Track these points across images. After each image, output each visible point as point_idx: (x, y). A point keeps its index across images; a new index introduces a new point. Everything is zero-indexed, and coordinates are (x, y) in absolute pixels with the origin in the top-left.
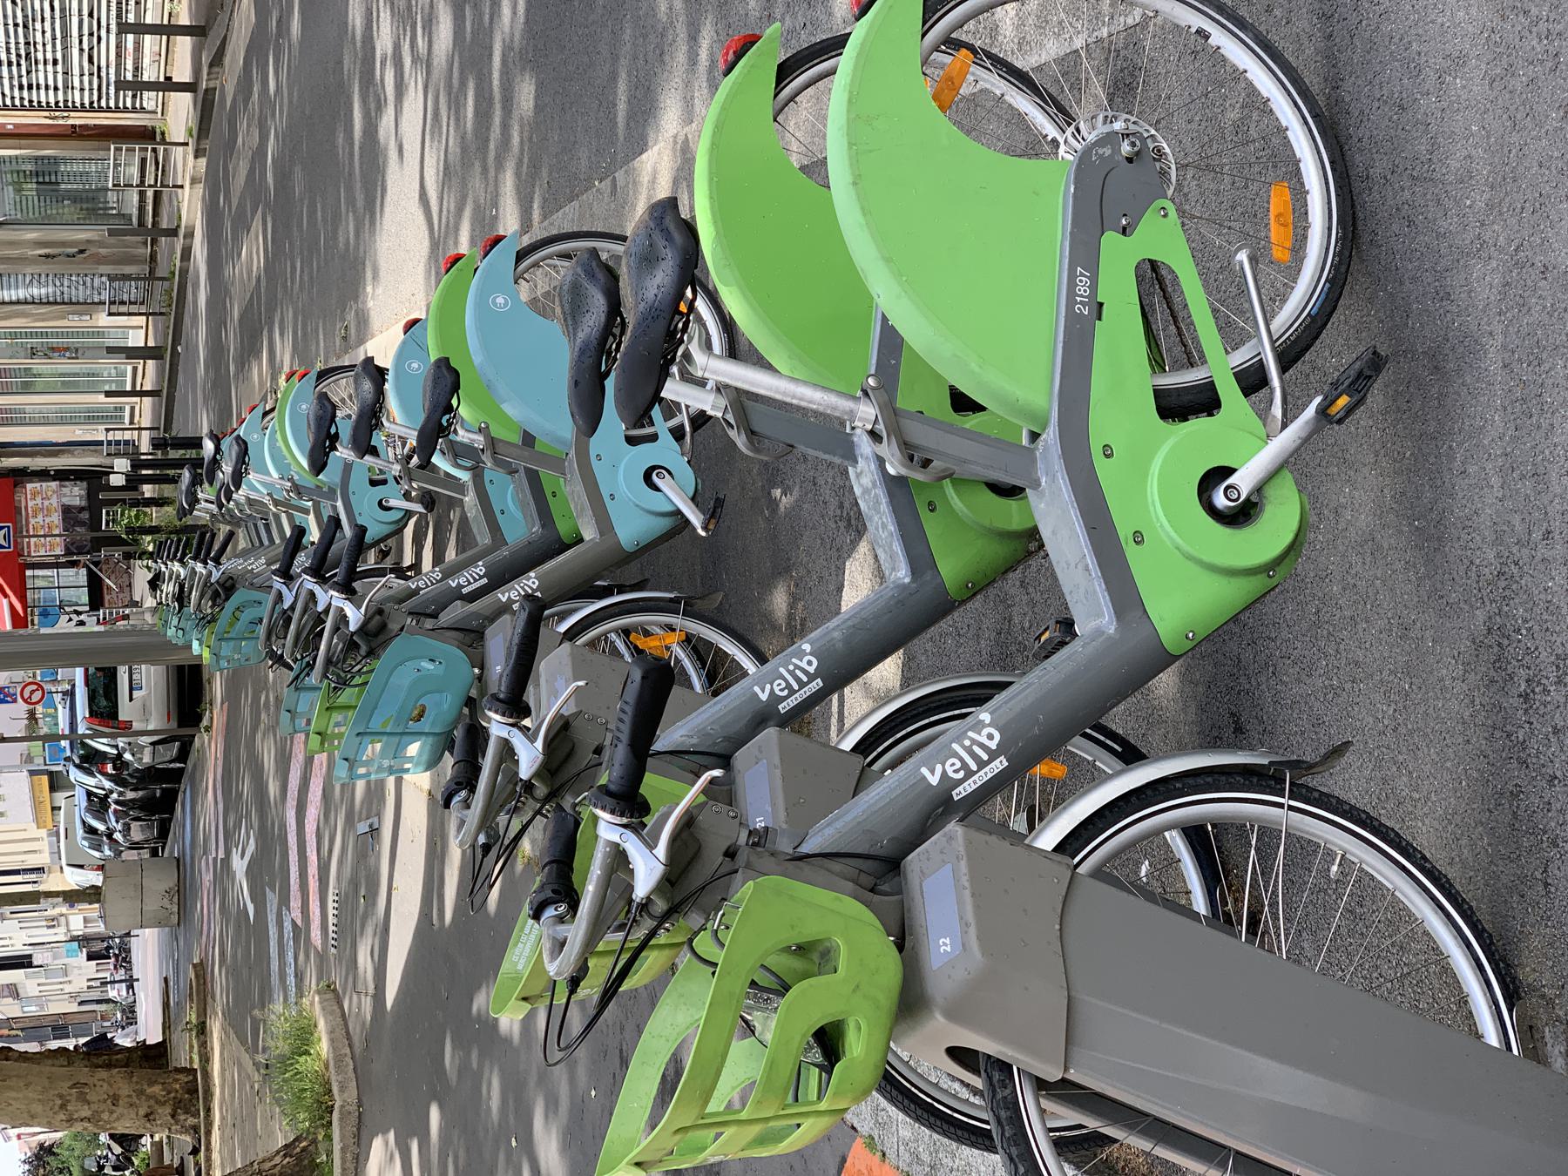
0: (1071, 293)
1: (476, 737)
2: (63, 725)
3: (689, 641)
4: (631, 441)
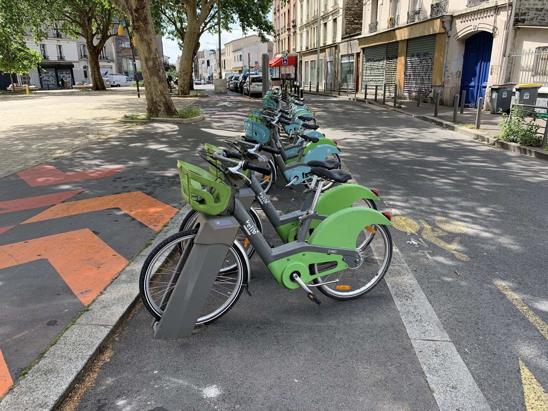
0: (332, 249)
1: (255, 142)
2: (251, 73)
3: (267, 183)
4: (303, 174)
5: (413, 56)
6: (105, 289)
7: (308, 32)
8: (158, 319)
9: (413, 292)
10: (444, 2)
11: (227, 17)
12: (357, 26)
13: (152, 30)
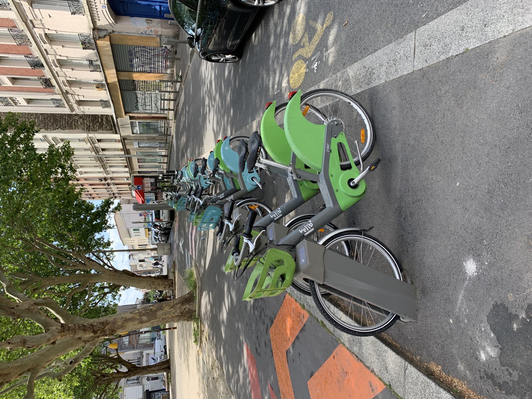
1: (222, 224)
3: (260, 208)
4: (249, 173)
5: (132, 66)
6: (368, 368)
7: (110, 166)
8: (397, 317)
9: (366, 68)
10: (80, 37)
11: (98, 243)
12: (104, 119)
13: (114, 317)
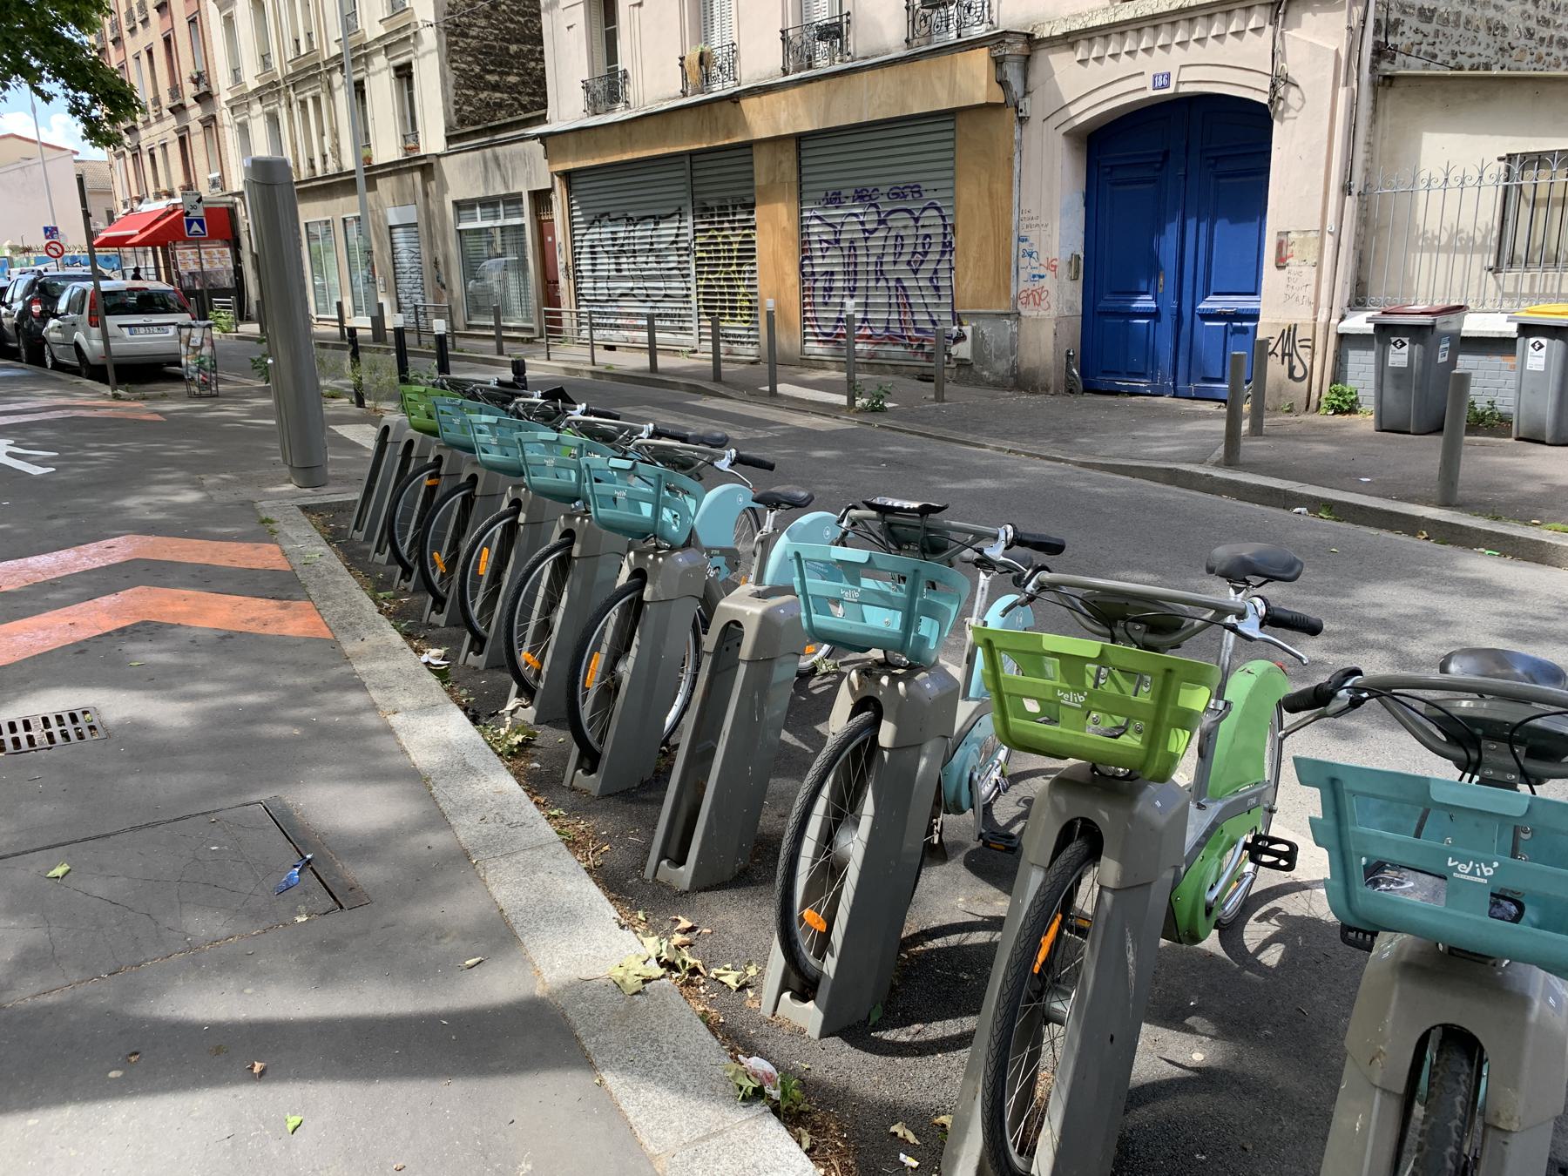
5: (835, 199)
7: (273, 119)
12: (498, 95)
